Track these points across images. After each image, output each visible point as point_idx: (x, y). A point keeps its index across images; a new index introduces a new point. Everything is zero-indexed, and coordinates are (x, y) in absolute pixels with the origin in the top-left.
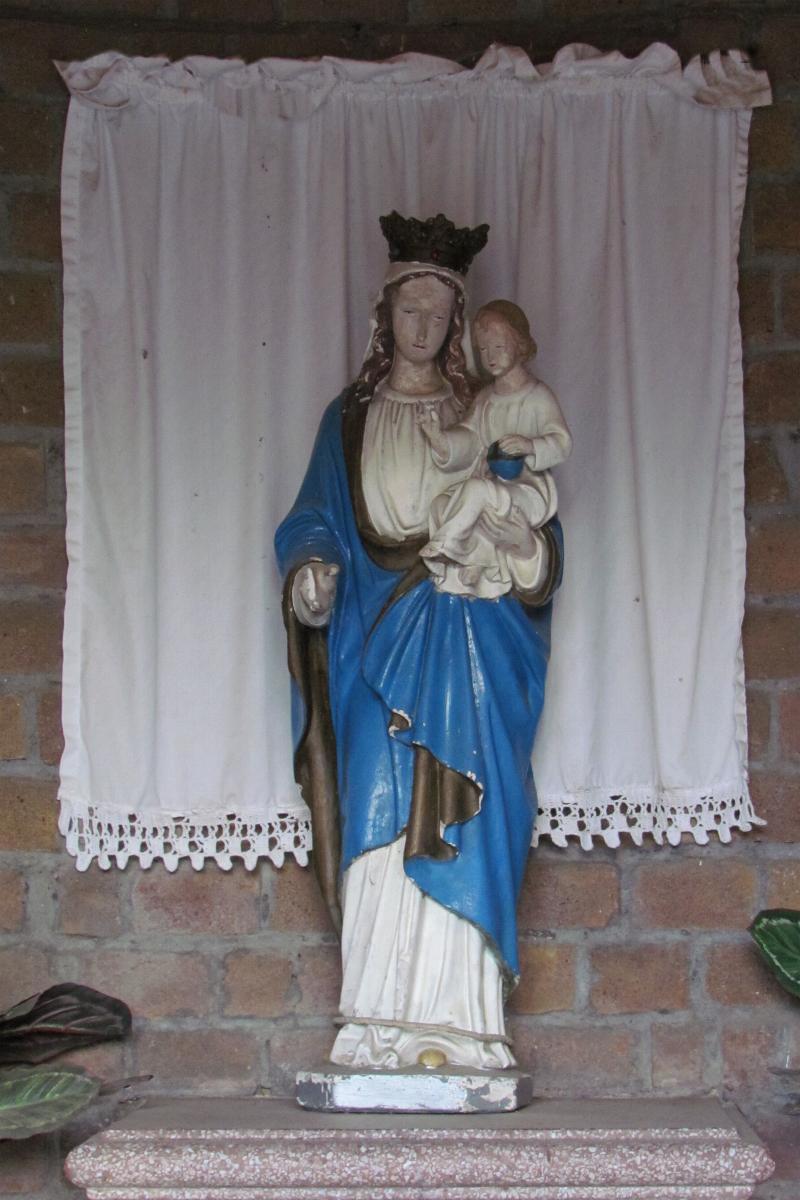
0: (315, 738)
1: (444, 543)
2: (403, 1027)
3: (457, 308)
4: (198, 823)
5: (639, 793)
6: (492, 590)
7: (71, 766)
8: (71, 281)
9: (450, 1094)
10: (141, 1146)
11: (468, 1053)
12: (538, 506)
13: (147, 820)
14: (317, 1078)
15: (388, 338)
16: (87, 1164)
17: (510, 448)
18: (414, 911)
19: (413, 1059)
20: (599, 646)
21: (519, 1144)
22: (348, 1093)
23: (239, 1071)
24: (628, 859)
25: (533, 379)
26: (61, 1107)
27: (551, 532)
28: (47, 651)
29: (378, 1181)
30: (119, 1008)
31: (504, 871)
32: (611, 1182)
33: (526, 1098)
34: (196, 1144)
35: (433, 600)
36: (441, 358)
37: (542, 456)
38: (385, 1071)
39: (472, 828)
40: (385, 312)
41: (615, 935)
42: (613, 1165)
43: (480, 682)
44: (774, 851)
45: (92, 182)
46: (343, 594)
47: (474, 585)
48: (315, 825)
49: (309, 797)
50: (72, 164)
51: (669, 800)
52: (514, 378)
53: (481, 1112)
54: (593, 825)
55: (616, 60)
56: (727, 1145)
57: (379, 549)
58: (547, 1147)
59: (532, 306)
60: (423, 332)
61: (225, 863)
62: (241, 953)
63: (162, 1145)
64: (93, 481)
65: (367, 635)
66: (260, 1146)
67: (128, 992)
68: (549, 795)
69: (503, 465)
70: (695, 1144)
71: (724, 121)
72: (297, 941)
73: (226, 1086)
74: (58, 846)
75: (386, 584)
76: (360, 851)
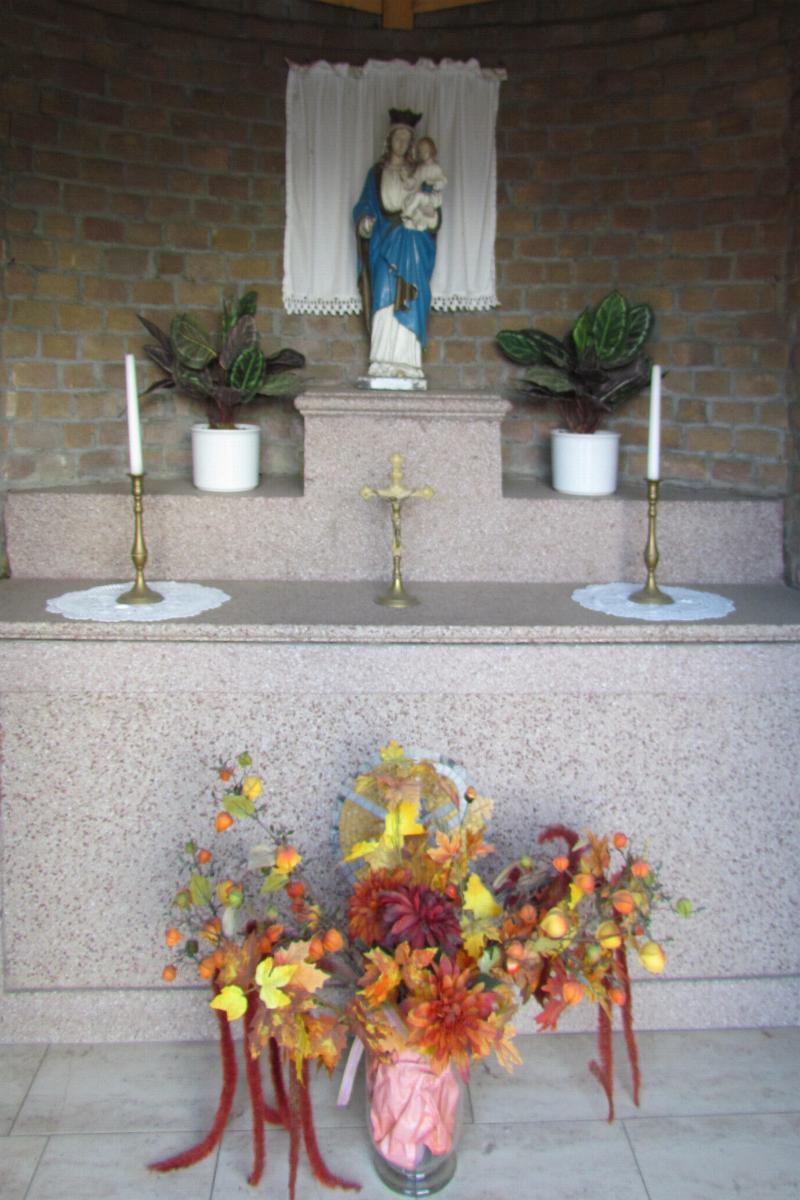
0: (365, 274)
1: (408, 212)
2: (392, 363)
3: (412, 139)
4: (325, 300)
5: (462, 294)
6: (421, 228)
7: (287, 281)
8: (289, 129)
9: (407, 385)
10: (317, 397)
11: (411, 372)
12: (437, 201)
13: (310, 298)
14: (365, 379)
15: (390, 147)
16: (301, 402)
17: (429, 183)
18: (395, 329)
19: (395, 373)
20: (450, 246)
21: (434, 399)
22: (376, 384)
23: (336, 378)
24: (457, 315)
25: (436, 162)
26: (289, 386)
27: (439, 210)
28: (280, 246)
29: (602, 354)
30: (302, 357)
31: (423, 316)
32: (462, 411)
33: (429, 388)
34: (334, 397)
35: (404, 231)
36: (406, 155)
37: (439, 185)
38: (386, 377)
39: (414, 303)
40: (390, 140)
41: (454, 338)
42: (464, 406)
43: (417, 258)
44: (502, 313)
45: (296, 97)
46: (377, 228)
47: (416, 226)
48: (363, 301)
49: (361, 292)
50: (290, 91)
51: (472, 297)
52: (430, 161)
53: (416, 390)
54: (448, 303)
55: (460, 64)
56: (497, 400)
57: (385, 214)
58: (443, 400)
59: (433, 136)
60: (401, 147)
61: (333, 313)
62: (337, 341)
63: (324, 397)
64: (295, 191)
65: (382, 242)
66: (354, 398)
67: (304, 351)
68: (436, 293)
69: (426, 188)
70: (488, 400)
71: (491, 85)
72: (356, 337)
73: (332, 383)
74: (281, 306)
75: (388, 225)
76: (378, 308)
